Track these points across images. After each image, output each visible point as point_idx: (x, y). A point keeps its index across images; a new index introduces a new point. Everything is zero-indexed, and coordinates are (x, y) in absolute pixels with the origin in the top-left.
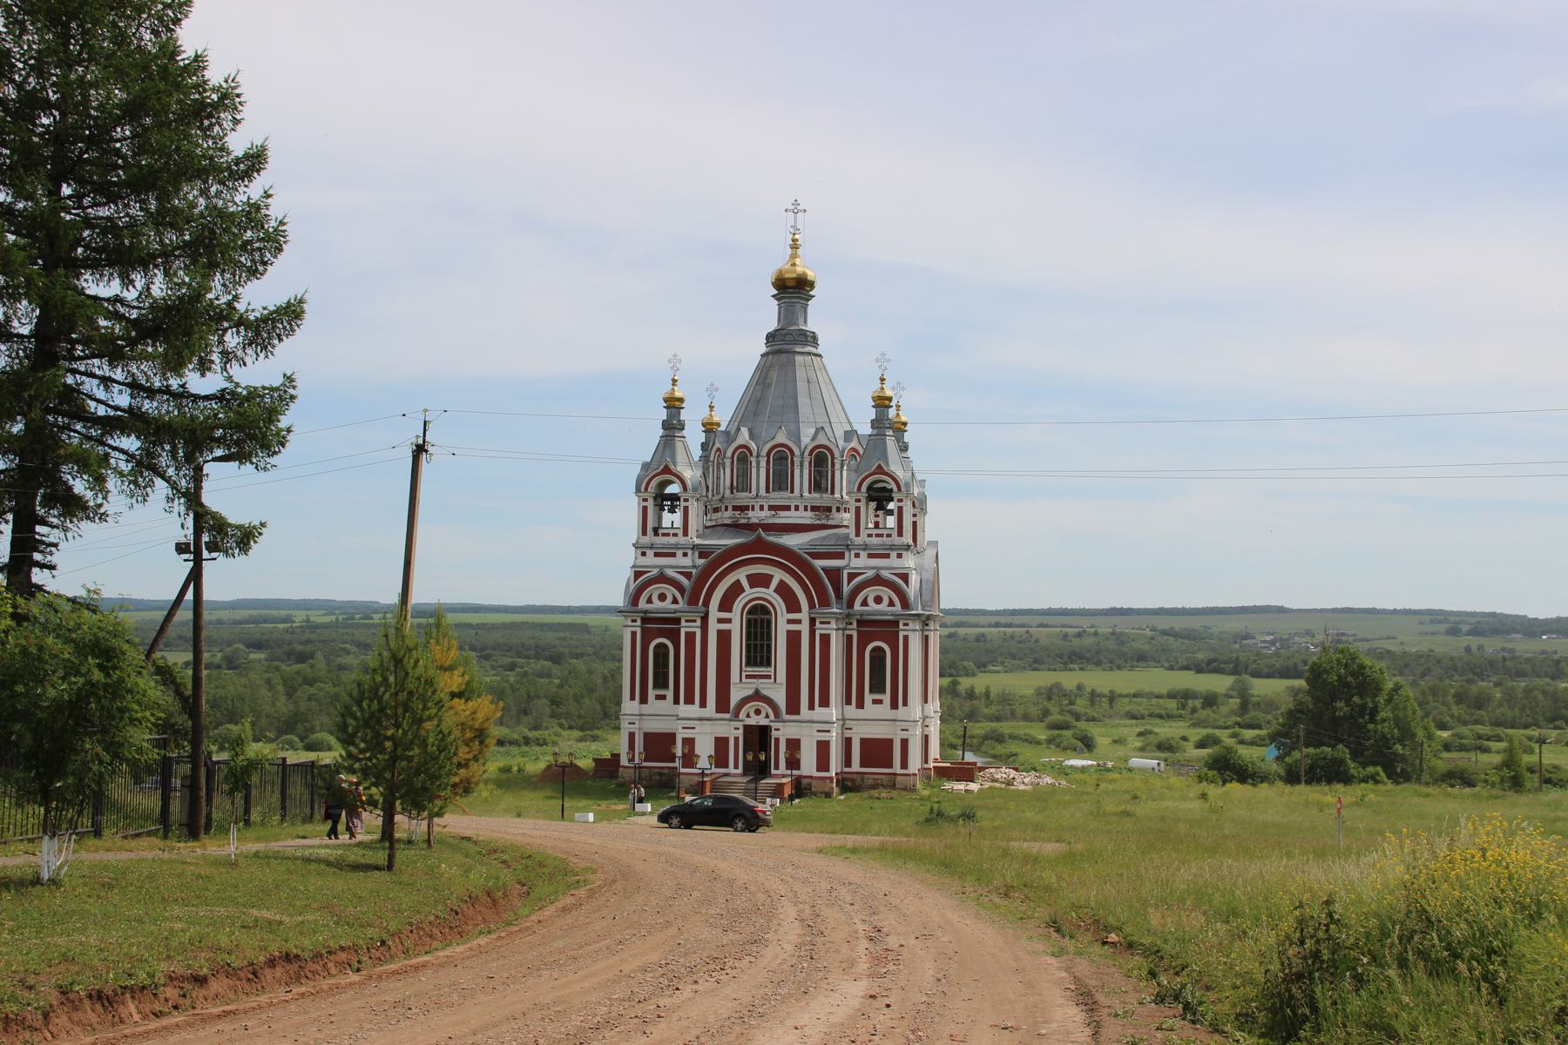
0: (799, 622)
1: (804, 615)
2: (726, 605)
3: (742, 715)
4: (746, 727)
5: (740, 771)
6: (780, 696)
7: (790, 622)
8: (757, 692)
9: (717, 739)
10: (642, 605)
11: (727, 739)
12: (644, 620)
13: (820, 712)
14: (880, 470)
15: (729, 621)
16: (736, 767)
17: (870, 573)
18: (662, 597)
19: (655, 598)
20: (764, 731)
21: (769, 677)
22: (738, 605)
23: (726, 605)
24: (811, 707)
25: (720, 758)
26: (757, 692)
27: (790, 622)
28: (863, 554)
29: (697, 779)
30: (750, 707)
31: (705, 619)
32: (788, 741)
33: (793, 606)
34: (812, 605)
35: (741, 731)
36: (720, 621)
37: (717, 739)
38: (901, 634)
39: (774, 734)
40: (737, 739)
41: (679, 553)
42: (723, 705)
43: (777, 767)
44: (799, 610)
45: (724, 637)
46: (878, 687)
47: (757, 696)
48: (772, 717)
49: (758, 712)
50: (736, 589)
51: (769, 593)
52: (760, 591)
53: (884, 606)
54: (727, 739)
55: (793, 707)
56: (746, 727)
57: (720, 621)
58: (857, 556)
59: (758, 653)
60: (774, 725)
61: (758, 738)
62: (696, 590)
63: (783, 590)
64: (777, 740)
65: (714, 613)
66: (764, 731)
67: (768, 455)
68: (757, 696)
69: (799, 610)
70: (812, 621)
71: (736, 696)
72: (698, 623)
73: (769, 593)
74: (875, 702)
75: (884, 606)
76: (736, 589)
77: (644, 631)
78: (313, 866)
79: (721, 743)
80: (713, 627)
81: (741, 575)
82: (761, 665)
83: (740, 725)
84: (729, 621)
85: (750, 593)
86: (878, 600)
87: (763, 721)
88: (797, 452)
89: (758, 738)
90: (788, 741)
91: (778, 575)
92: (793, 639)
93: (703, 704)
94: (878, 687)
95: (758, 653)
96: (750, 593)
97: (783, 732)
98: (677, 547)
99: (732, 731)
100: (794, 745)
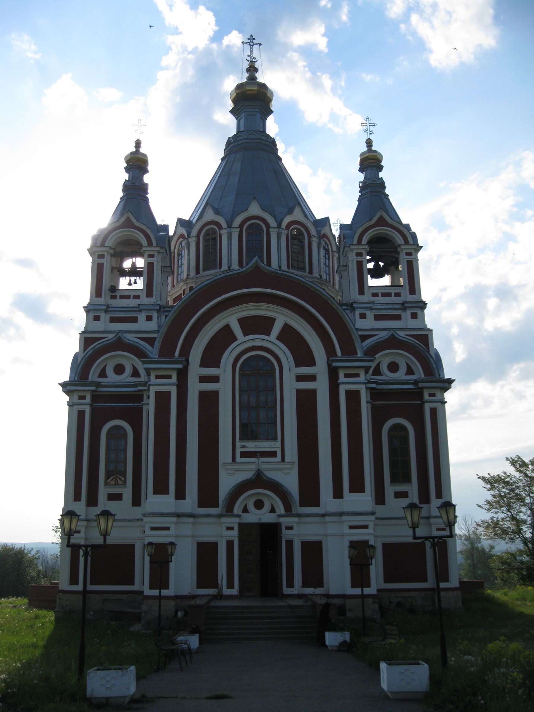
0: (312, 378)
1: (320, 368)
2: (211, 357)
3: (237, 509)
4: (242, 526)
5: (235, 591)
6: (291, 481)
7: (300, 378)
8: (259, 474)
9: (200, 545)
10: (93, 376)
11: (214, 545)
12: (96, 397)
13: (353, 501)
14: (382, 222)
15: (215, 379)
16: (230, 585)
17: (383, 335)
18: (119, 369)
19: (110, 371)
20: (269, 533)
21: (273, 454)
22: (228, 358)
23: (211, 357)
24: (338, 493)
25: (206, 572)
26: (259, 474)
27: (300, 378)
28: (370, 315)
29: (323, 601)
30: (247, 498)
31: (183, 375)
32: (304, 544)
33: (304, 357)
34: (330, 351)
35: (235, 533)
36: (203, 379)
37: (200, 545)
38: (427, 407)
39: (286, 534)
40: (230, 544)
41: (142, 317)
42: (208, 495)
43: (291, 584)
44: (312, 362)
45: (209, 401)
46: (401, 475)
47: (259, 481)
48: (281, 509)
49: (259, 505)
50: (225, 337)
51: (271, 340)
52: (256, 339)
53: (401, 375)
54: (214, 545)
55: (310, 494)
56: (242, 526)
57: (203, 379)
58: (363, 316)
59: (256, 424)
60: (285, 521)
61: (264, 542)
62: (172, 342)
63: (289, 335)
64: (290, 543)
65: (195, 370)
66: (269, 533)
67: (241, 226)
68: (259, 481)
69: (312, 362)
70: (333, 373)
71: (227, 481)
72: (174, 379)
73: (271, 340)
74: (399, 495)
75: (401, 375)
76: (225, 337)
77: (94, 411)
78: (327, 519)
79: (206, 552)
80: (194, 388)
81: (232, 318)
82: (267, 439)
83: (234, 522)
84: (215, 379)
85: (243, 341)
86: (393, 367)
87: (264, 516)
88: (273, 223)
89: (264, 542)
90: (304, 544)
91: (282, 318)
92: (306, 401)
93: (180, 495)
94: (401, 475)
95: (256, 424)
96: (243, 341)
97: (300, 530)
98: (139, 309)
99: (221, 531)
100: (313, 551)
